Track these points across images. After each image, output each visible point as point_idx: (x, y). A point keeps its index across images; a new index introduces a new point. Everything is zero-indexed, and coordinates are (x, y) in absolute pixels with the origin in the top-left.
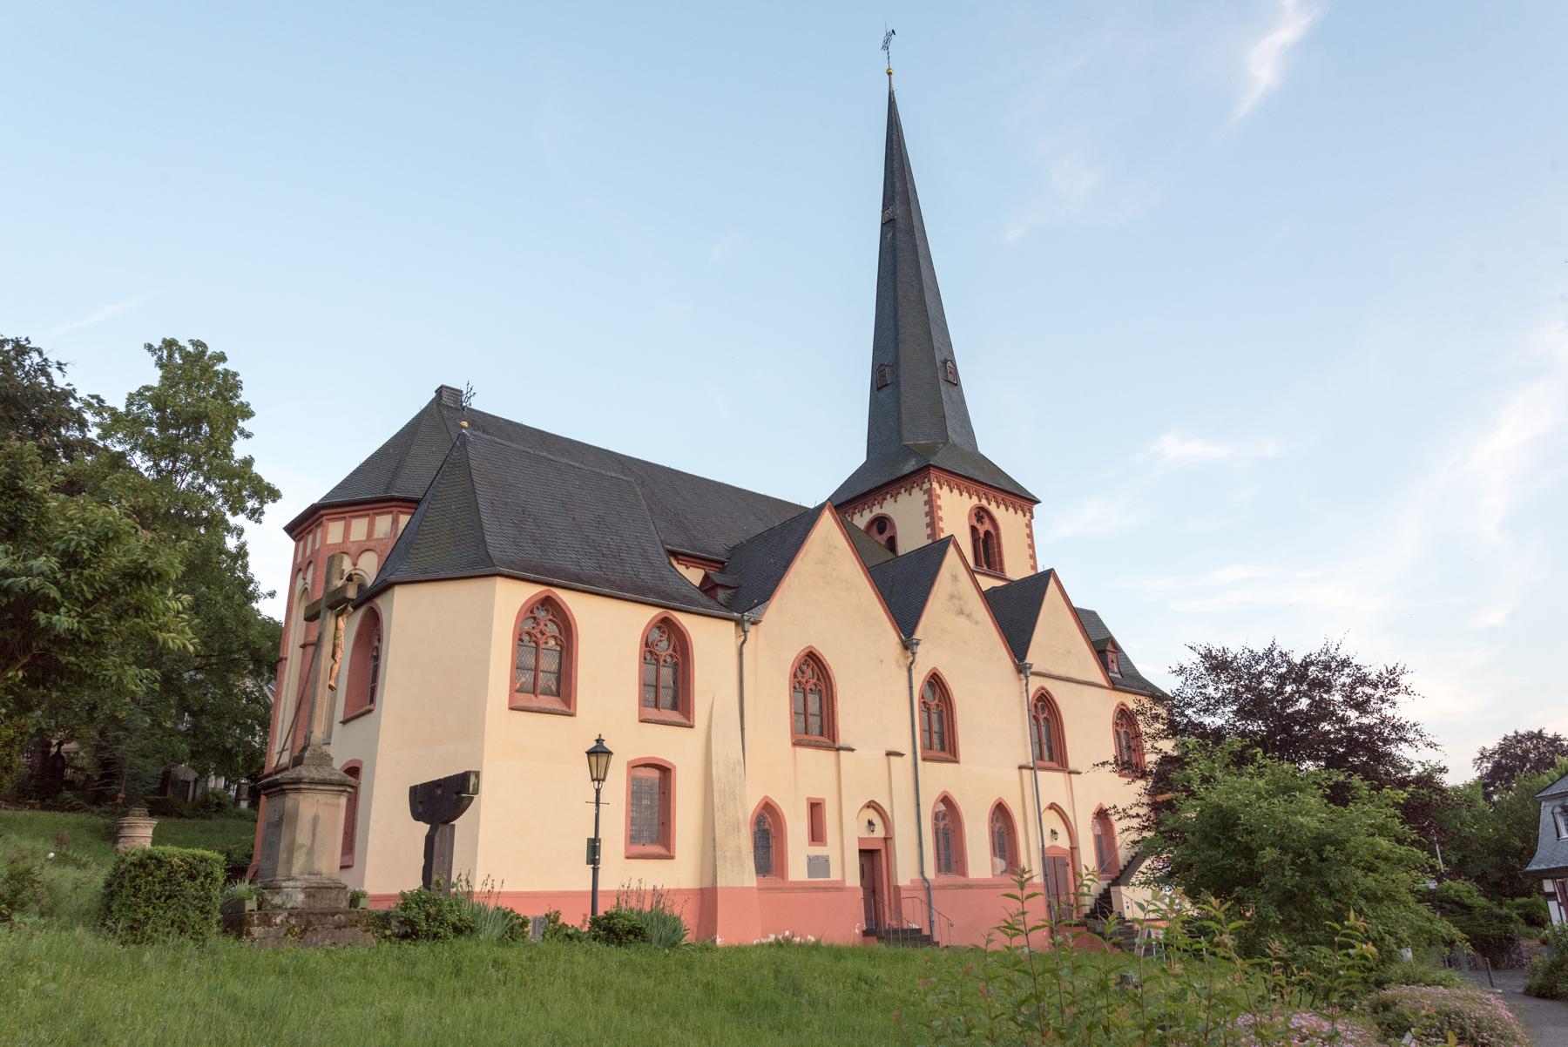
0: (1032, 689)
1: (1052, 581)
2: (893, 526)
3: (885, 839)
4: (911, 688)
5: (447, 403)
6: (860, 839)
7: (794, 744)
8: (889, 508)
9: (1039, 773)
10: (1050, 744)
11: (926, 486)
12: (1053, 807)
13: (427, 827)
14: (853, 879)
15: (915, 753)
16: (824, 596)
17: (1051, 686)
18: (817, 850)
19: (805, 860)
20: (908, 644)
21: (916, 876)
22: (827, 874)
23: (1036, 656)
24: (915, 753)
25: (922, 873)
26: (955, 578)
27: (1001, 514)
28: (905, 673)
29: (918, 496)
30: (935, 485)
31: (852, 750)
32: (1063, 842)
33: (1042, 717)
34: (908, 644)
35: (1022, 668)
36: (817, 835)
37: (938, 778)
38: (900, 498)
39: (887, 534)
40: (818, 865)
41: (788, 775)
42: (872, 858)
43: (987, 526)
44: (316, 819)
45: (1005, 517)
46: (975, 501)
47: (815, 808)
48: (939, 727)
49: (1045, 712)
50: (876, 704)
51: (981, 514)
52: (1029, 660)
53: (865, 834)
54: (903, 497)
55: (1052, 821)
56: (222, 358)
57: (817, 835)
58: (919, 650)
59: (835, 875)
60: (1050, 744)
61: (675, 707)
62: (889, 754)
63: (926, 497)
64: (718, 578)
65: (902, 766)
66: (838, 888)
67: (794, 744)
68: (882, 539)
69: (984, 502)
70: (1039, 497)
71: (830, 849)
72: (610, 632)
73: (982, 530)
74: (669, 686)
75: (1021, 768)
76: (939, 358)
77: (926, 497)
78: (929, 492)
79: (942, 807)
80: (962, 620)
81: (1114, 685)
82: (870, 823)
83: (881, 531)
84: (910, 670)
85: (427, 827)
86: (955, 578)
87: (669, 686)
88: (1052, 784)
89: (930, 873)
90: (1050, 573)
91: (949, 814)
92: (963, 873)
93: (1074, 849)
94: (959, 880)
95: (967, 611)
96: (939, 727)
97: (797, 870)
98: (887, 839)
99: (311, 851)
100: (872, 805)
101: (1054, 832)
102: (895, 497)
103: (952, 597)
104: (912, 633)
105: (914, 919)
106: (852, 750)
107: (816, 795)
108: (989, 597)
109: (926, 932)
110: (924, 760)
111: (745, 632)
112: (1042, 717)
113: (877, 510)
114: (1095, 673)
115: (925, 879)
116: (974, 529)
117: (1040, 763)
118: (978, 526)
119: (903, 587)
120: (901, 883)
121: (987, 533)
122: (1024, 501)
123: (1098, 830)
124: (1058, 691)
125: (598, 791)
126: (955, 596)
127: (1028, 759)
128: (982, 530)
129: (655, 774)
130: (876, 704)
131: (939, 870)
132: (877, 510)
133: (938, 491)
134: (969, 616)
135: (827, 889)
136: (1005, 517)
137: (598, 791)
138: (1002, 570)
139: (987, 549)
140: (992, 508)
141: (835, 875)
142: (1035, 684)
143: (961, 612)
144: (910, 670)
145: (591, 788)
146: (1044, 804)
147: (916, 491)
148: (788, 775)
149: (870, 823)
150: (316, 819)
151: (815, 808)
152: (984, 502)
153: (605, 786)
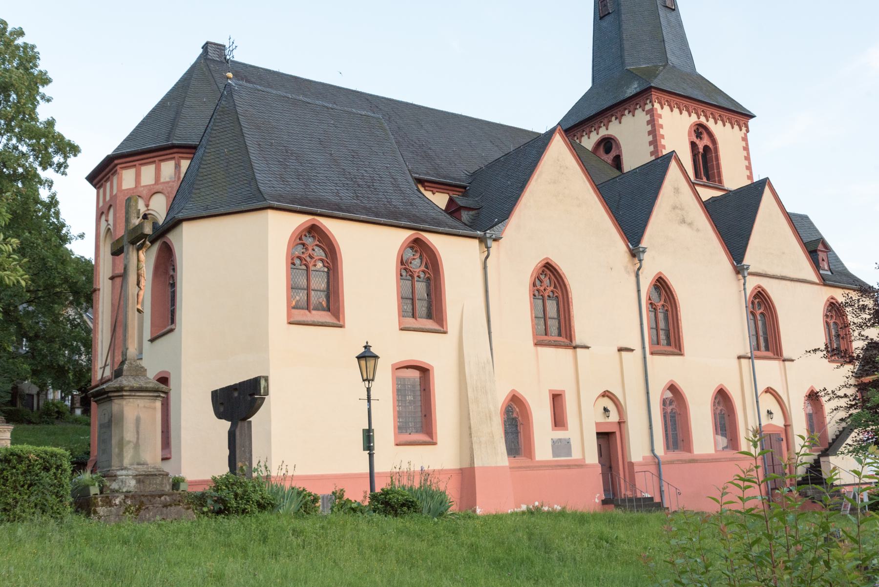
1: (767, 190)
2: (618, 146)
3: (619, 423)
4: (639, 291)
5: (213, 58)
6: (597, 424)
7: (536, 344)
9: (756, 362)
10: (765, 333)
11: (648, 107)
12: (769, 390)
13: (229, 423)
14: (592, 457)
15: (644, 348)
17: (766, 284)
18: (560, 434)
19: (550, 443)
20: (635, 252)
21: (647, 453)
23: (748, 259)
24: (644, 348)
25: (652, 450)
26: (677, 190)
28: (633, 278)
29: (641, 117)
30: (657, 105)
31: (588, 348)
32: (778, 421)
33: (758, 312)
34: (635, 252)
35: (739, 269)
36: (559, 421)
37: (665, 369)
38: (624, 119)
39: (613, 154)
40: (561, 447)
41: (538, 372)
43: (706, 141)
44: (138, 421)
45: (724, 133)
46: (694, 118)
47: (557, 398)
48: (664, 321)
49: (761, 307)
50: (606, 303)
51: (700, 130)
52: (746, 262)
53: (601, 419)
54: (627, 119)
55: (768, 403)
56: (21, 33)
57: (559, 421)
58: (646, 257)
59: (576, 455)
60: (765, 333)
61: (429, 316)
62: (620, 350)
63: (648, 117)
64: (461, 201)
65: (633, 360)
66: (580, 465)
67: (536, 344)
70: (753, 112)
71: (571, 433)
72: (370, 253)
73: (701, 145)
74: (424, 296)
75: (739, 358)
77: (648, 117)
78: (651, 112)
79: (669, 395)
80: (684, 228)
81: (825, 281)
82: (606, 410)
83: (608, 151)
84: (637, 276)
85: (229, 423)
86: (677, 190)
87: (424, 296)
88: (768, 371)
89: (660, 450)
90: (764, 182)
91: (675, 402)
92: (688, 448)
94: (685, 455)
95: (688, 220)
96: (664, 321)
97: (543, 451)
99: (137, 446)
100: (606, 394)
102: (619, 119)
104: (639, 242)
105: (646, 488)
106: (588, 348)
107: (557, 388)
108: (710, 208)
109: (657, 499)
110: (652, 353)
111: (488, 248)
112: (758, 312)
113: (603, 132)
114: (807, 271)
115: (655, 456)
116: (693, 145)
117: (757, 353)
118: (698, 142)
119: (629, 200)
120: (633, 460)
121: (706, 148)
122: (739, 115)
123: (810, 409)
124: (773, 289)
125: (369, 390)
127: (746, 350)
128: (701, 145)
129: (416, 374)
130: (606, 303)
131: (668, 447)
133: (659, 111)
135: (568, 466)
136: (724, 133)
137: (369, 390)
138: (720, 182)
139: (706, 163)
140: (711, 124)
141: (576, 455)
142: (752, 283)
143: (683, 221)
144: (637, 276)
145: (363, 386)
146: (761, 388)
147: (639, 112)
148: (538, 372)
149: (606, 410)
150: (138, 421)
151: (557, 398)
152: (703, 119)
153: (374, 386)
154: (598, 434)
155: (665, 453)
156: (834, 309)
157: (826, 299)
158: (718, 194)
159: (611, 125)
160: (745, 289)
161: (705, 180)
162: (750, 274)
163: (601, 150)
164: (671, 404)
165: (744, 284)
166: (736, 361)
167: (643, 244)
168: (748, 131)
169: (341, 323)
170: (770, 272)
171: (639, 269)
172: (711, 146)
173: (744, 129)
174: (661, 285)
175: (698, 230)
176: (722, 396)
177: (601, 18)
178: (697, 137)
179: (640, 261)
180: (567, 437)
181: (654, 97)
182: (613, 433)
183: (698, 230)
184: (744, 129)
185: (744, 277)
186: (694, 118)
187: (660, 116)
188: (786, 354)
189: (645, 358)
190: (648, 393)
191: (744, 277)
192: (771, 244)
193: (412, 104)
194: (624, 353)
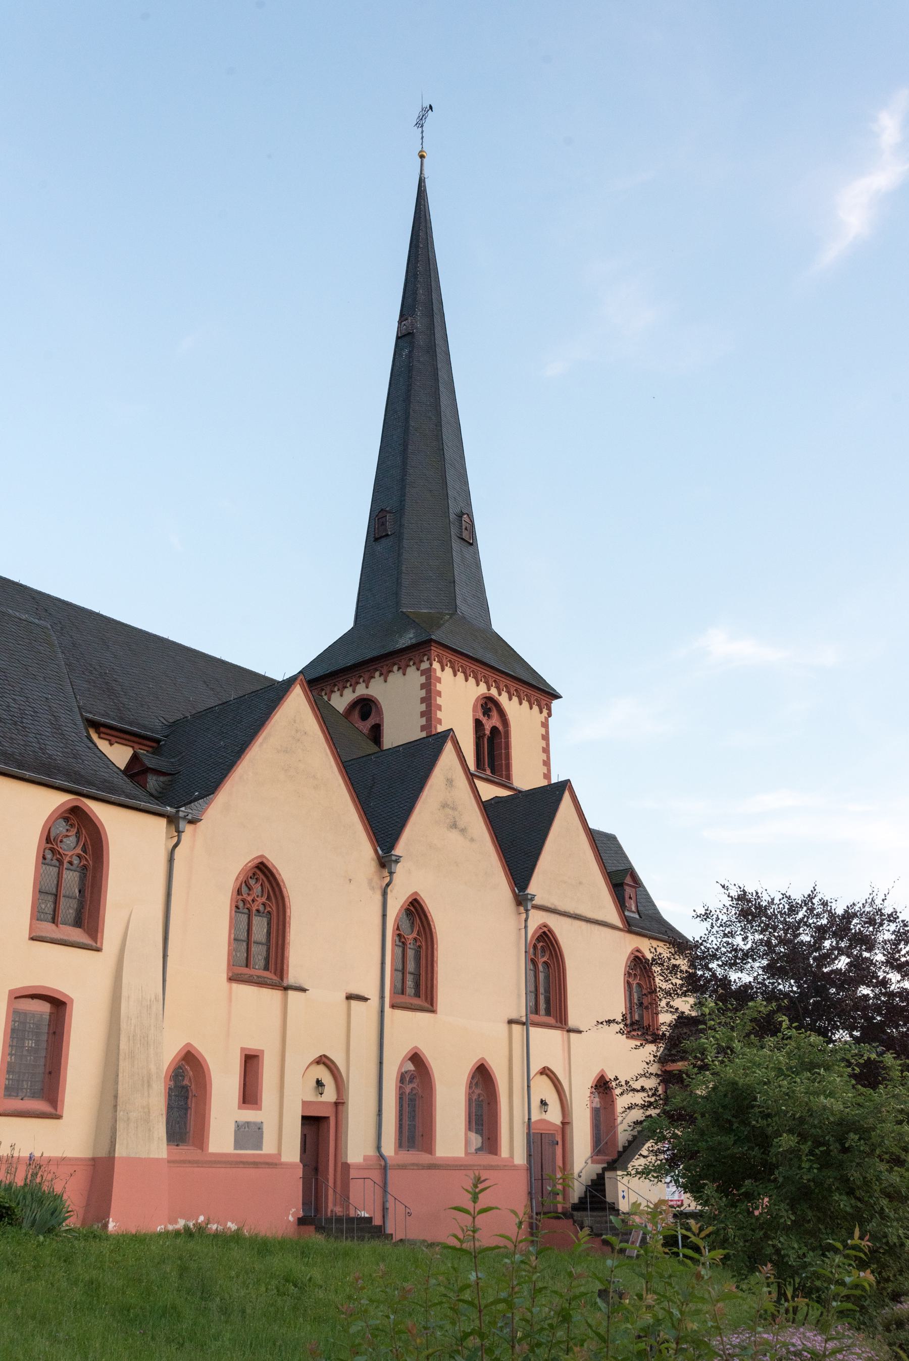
0: (533, 926)
2: (380, 712)
3: (337, 1104)
4: (384, 916)
6: (305, 1103)
7: (231, 979)
8: (377, 688)
9: (533, 1030)
11: (424, 666)
12: (546, 1072)
15: (382, 997)
16: (286, 795)
18: (249, 1115)
20: (386, 861)
21: (371, 1151)
22: (259, 1147)
24: (382, 997)
25: (379, 1148)
26: (450, 782)
27: (513, 708)
28: (378, 897)
29: (414, 677)
30: (436, 665)
31: (304, 990)
32: (554, 1116)
34: (386, 861)
35: (522, 899)
36: (249, 1095)
37: (409, 1030)
38: (391, 678)
39: (371, 721)
40: (249, 1134)
42: (317, 1128)
43: (495, 721)
45: (519, 713)
46: (482, 689)
48: (414, 972)
50: (338, 932)
51: (488, 705)
53: (311, 1097)
54: (395, 677)
57: (249, 1095)
58: (399, 869)
59: (268, 1147)
62: (350, 997)
63: (423, 679)
64: (150, 761)
65: (364, 1014)
66: (272, 1163)
67: (231, 979)
68: (365, 727)
69: (494, 692)
73: (488, 725)
75: (511, 1022)
76: (453, 509)
77: (423, 679)
79: (410, 1067)
81: (630, 927)
82: (319, 1083)
83: (365, 716)
84: (385, 894)
86: (450, 782)
88: (547, 1043)
89: (389, 1148)
91: (418, 1073)
93: (566, 1124)
95: (461, 824)
96: (414, 972)
97: (220, 1138)
98: (339, 1105)
100: (323, 1061)
101: (543, 1103)
102: (385, 676)
103: (444, 806)
105: (363, 1206)
106: (304, 990)
107: (253, 1045)
108: (490, 809)
110: (393, 1006)
112: (541, 960)
113: (361, 690)
115: (381, 1156)
116: (478, 724)
118: (484, 720)
119: (385, 787)
120: (349, 1161)
121: (494, 729)
122: (541, 694)
124: (563, 930)
126: (449, 803)
127: (519, 1010)
128: (488, 725)
129: (44, 1008)
130: (338, 932)
132: (361, 690)
133: (439, 673)
134: (463, 831)
136: (519, 713)
138: (509, 777)
139: (493, 750)
140: (503, 699)
141: (268, 1147)
142: (536, 919)
143: (454, 826)
144: (385, 894)
146: (535, 1068)
147: (412, 671)
148: (220, 1018)
149: (319, 1083)
151: (251, 1062)
152: (494, 692)
154: (306, 1119)
155: (396, 1153)
156: (639, 966)
157: (629, 951)
158: (504, 793)
159: (373, 683)
160: (526, 927)
161: (488, 772)
162: (536, 907)
163: (356, 714)
164: (411, 1081)
165: (526, 920)
166: (505, 1026)
167: (398, 851)
168: (550, 715)
169: (99, 945)
170: (562, 907)
171: (388, 885)
172: (501, 728)
173: (545, 712)
174: (416, 910)
175: (472, 840)
176: (482, 1075)
177: (376, 540)
178: (484, 714)
179: (391, 873)
180: (258, 1120)
181: (433, 654)
182: (326, 1119)
183: (472, 840)
184: (545, 712)
185: (527, 911)
186: (482, 689)
187: (439, 680)
188: (572, 1022)
189: (382, 1011)
190: (381, 1063)
191: (527, 911)
192: (565, 870)
193: (98, 614)
194: (354, 1003)
